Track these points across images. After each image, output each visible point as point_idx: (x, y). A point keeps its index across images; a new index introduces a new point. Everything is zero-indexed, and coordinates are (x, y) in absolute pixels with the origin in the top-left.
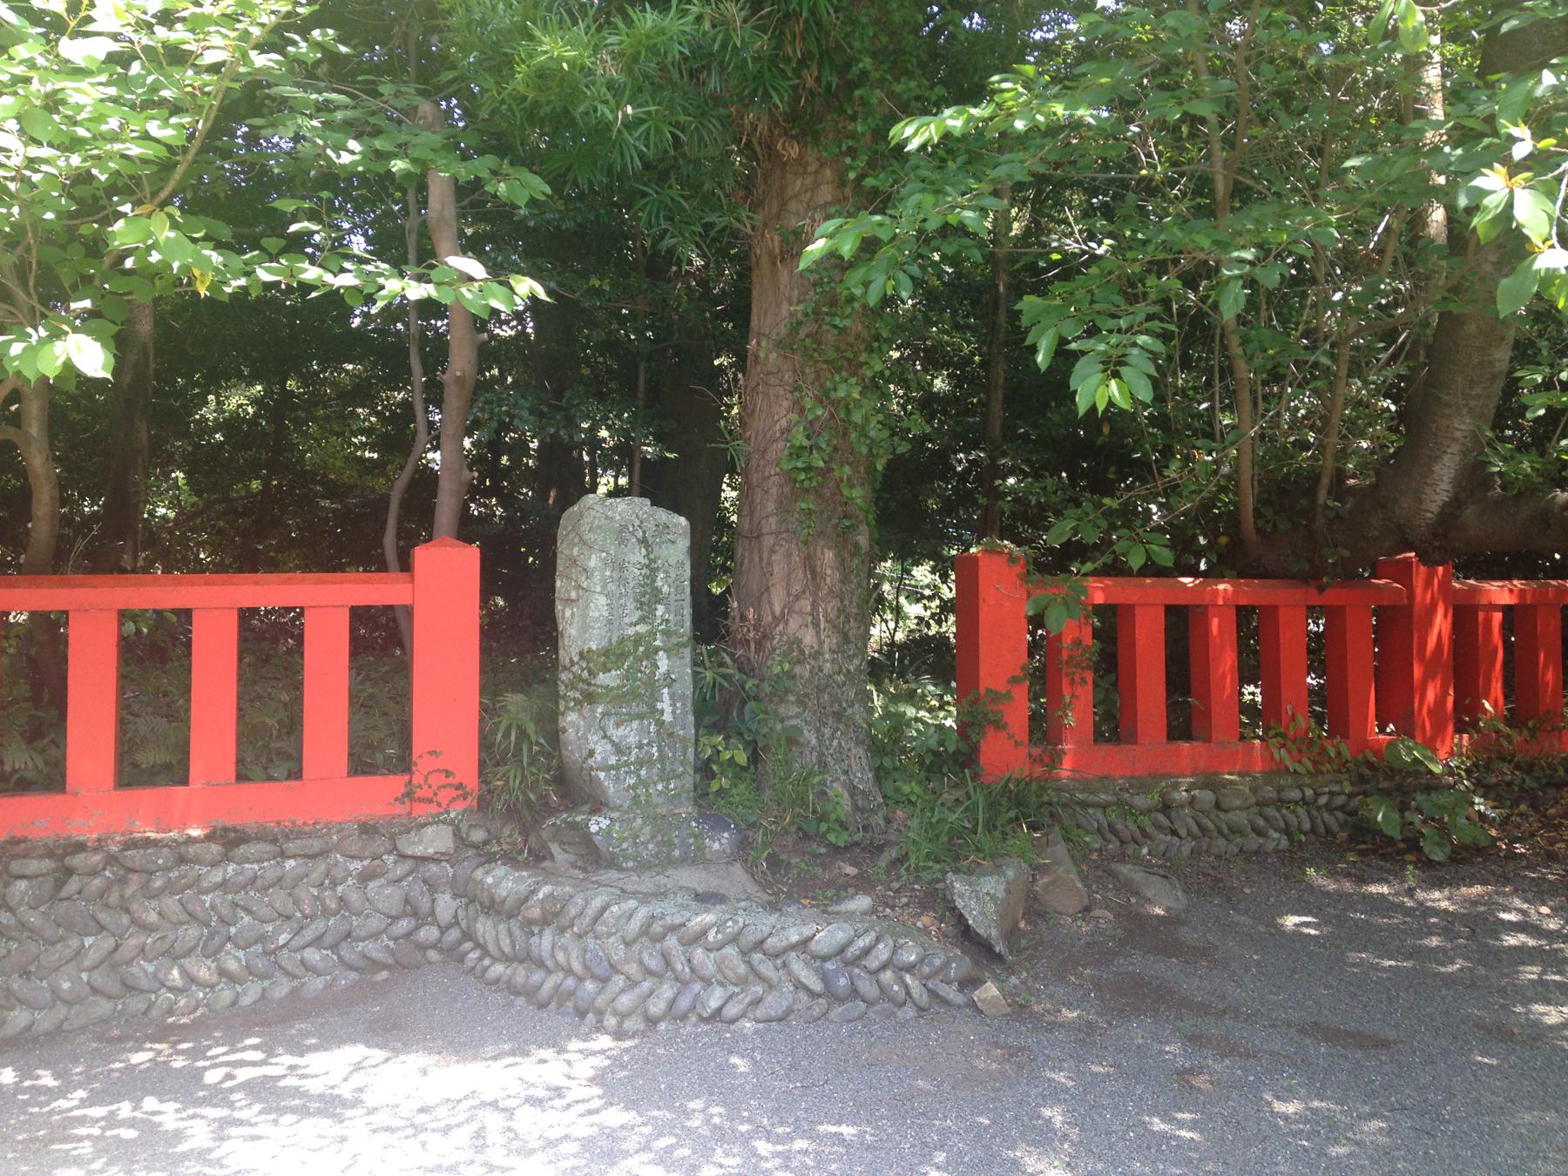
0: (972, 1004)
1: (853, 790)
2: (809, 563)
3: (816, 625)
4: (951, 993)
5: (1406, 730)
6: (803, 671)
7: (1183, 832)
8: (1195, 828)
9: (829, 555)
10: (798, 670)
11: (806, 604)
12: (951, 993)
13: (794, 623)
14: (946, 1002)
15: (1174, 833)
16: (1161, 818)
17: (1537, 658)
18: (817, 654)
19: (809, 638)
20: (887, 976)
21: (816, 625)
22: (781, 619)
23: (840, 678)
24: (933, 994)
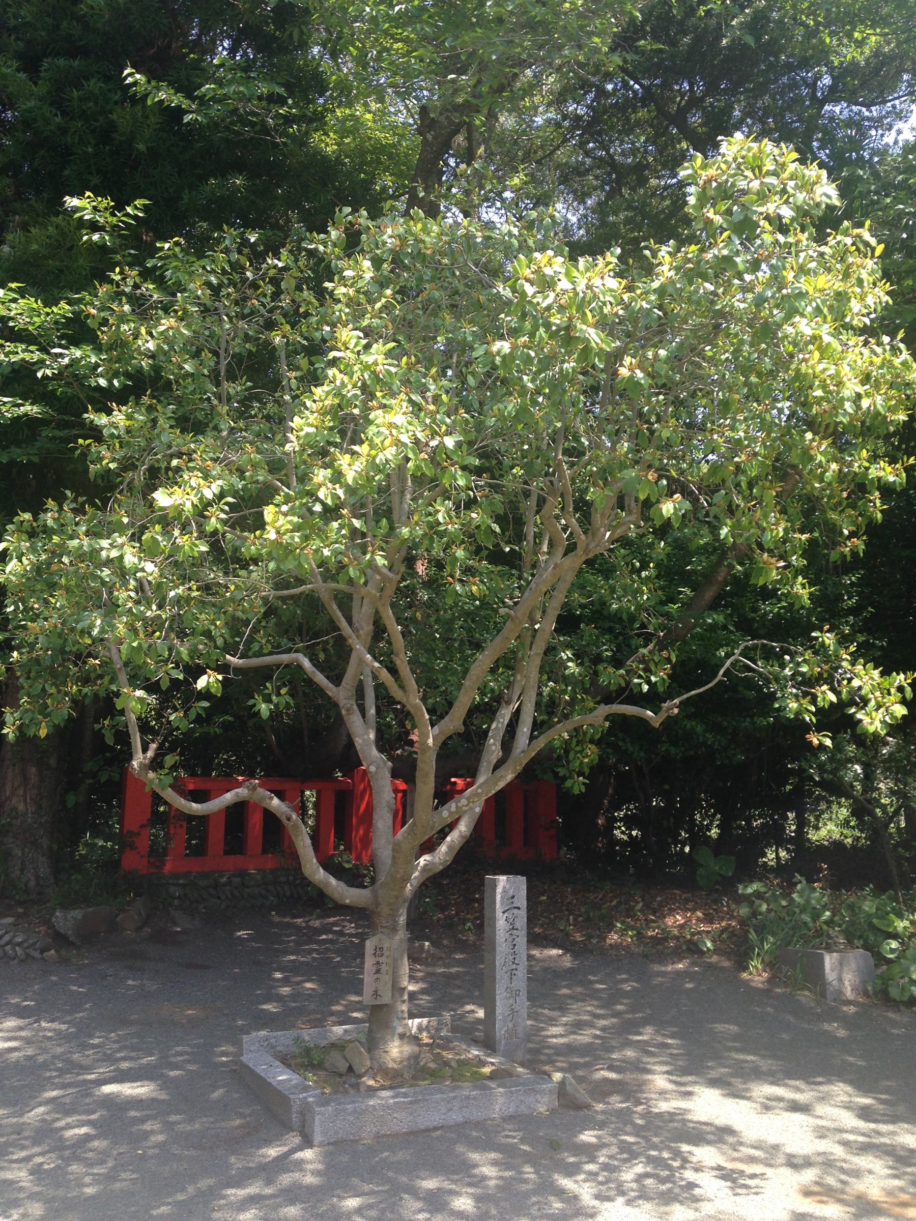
0: (43, 959)
1: (37, 877)
2: (708, 1067)
3: (25, 801)
4: (36, 954)
5: (348, 848)
6: (17, 822)
7: (223, 898)
8: (229, 895)
9: (33, 770)
10: (14, 821)
11: (21, 792)
12: (36, 954)
13: (14, 800)
14: (33, 958)
15: (219, 898)
16: (212, 891)
17: (750, 1054)
18: (25, 814)
19: (21, 807)
20: (8, 948)
21: (25, 801)
22: (9, 798)
23: (36, 826)
24: (28, 955)
